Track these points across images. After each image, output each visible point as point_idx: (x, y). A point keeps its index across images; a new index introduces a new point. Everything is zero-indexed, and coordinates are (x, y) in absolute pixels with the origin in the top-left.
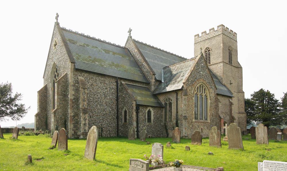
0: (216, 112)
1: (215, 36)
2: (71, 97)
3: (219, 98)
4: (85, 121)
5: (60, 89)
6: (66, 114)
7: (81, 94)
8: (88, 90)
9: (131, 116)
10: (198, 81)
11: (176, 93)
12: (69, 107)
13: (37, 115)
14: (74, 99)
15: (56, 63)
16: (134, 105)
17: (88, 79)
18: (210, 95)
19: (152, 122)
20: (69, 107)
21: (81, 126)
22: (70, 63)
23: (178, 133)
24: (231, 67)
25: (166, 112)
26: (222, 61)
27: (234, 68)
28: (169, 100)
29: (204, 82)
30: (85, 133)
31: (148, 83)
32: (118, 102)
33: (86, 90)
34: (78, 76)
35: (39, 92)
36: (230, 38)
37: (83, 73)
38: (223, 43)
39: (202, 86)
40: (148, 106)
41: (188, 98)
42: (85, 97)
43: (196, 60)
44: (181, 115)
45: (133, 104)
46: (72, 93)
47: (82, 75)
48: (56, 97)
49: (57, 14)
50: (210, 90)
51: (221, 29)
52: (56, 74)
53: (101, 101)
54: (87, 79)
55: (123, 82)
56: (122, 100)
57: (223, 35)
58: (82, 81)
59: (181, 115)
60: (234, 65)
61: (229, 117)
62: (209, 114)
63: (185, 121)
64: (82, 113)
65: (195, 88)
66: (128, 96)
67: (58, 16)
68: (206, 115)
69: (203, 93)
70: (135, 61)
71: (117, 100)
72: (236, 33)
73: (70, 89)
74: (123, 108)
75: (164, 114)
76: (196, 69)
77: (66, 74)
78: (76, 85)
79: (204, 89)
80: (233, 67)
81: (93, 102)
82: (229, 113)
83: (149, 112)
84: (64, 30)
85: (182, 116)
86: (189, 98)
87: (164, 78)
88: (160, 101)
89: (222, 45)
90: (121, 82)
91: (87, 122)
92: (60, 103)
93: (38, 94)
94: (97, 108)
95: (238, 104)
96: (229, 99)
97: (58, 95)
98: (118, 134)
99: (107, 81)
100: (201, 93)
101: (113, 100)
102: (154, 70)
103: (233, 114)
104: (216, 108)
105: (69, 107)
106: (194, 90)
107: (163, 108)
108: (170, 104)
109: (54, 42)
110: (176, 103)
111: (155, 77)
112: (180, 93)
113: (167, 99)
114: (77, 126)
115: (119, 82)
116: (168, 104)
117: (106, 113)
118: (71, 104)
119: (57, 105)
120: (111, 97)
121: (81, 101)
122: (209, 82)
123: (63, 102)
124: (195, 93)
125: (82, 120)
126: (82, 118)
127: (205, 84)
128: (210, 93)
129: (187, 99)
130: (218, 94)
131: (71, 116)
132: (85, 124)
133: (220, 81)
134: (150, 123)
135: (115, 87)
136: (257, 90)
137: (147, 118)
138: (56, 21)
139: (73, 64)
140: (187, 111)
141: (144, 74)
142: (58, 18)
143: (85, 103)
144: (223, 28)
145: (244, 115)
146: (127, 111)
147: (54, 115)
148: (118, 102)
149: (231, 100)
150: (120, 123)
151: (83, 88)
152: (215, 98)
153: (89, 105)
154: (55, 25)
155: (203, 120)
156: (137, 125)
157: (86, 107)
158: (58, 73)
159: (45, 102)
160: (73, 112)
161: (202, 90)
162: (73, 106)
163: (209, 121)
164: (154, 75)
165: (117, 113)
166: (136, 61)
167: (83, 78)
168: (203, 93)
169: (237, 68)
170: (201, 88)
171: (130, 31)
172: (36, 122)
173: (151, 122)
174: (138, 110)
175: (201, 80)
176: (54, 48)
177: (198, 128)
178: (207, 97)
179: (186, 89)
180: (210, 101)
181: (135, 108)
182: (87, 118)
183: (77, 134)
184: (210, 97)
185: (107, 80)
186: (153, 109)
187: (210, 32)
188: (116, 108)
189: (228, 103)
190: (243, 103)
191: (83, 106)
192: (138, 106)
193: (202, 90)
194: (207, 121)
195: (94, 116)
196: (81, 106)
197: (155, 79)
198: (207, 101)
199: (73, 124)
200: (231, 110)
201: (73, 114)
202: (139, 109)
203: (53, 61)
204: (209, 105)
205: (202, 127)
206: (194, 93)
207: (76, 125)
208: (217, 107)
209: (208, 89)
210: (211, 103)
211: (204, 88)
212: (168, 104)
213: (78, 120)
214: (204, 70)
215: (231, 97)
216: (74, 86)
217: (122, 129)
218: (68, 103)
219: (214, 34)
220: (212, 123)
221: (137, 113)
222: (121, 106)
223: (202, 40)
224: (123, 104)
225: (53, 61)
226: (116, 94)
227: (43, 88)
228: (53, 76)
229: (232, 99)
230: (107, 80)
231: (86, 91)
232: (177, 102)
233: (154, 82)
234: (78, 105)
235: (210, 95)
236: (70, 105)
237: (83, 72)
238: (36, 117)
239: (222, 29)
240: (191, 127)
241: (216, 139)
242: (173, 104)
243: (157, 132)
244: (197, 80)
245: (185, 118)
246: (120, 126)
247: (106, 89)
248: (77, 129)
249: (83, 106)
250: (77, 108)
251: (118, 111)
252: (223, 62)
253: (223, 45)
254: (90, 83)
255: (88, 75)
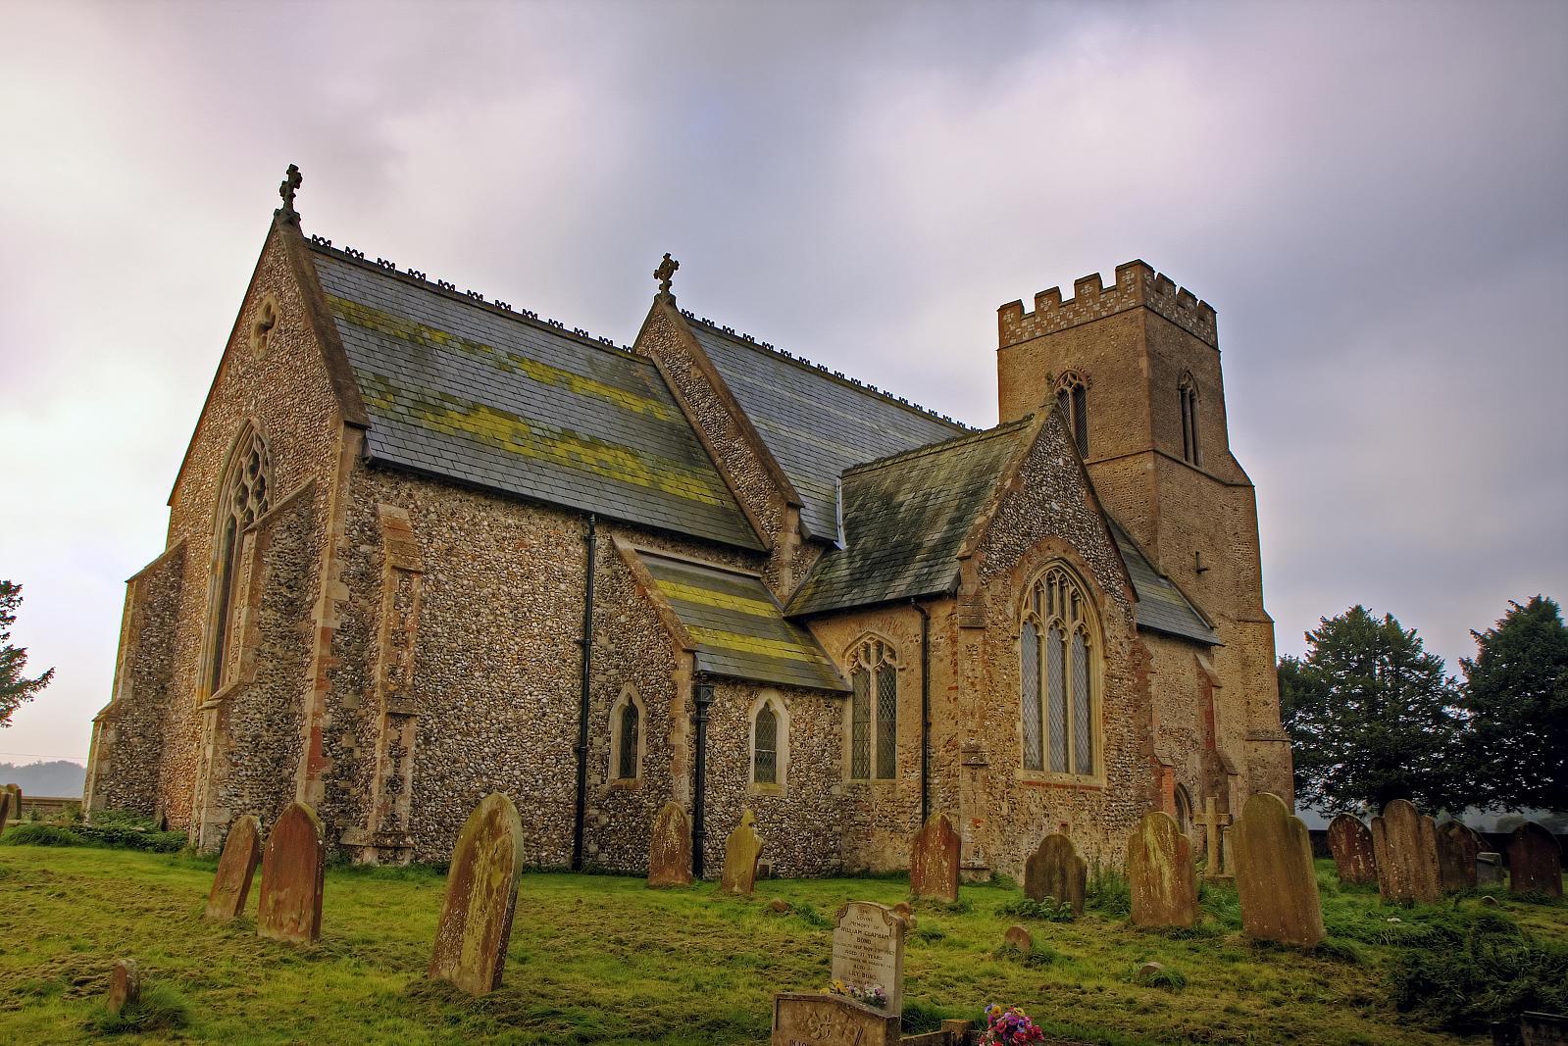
0: (1139, 727)
1: (1104, 314)
2: (326, 615)
3: (1152, 646)
4: (397, 766)
5: (268, 571)
6: (289, 717)
7: (385, 602)
8: (426, 581)
9: (665, 739)
10: (1040, 550)
11: (922, 612)
12: (308, 677)
13: (106, 719)
14: (342, 631)
15: (255, 421)
16: (683, 676)
17: (433, 516)
18: (1103, 629)
19: (782, 776)
20: (312, 673)
21: (367, 791)
22: (343, 426)
23: (943, 848)
24: (1194, 479)
25: (859, 724)
26: (1147, 446)
27: (1213, 484)
28: (880, 653)
29: (1070, 558)
30: (390, 836)
31: (760, 556)
32: (586, 657)
33: (416, 579)
34: (376, 501)
35: (136, 583)
36: (1185, 330)
37: (409, 485)
38: (1149, 354)
39: (1058, 576)
40: (763, 685)
41: (985, 643)
42: (411, 619)
43: (1022, 434)
44: (951, 744)
45: (676, 667)
46: (334, 596)
47: (397, 496)
48: (240, 615)
49: (293, 171)
50: (1103, 604)
51: (1134, 281)
52: (250, 483)
53: (492, 649)
54: (425, 516)
55: (624, 544)
56: (612, 647)
57: (1145, 314)
58: (395, 527)
59: (951, 744)
60: (1211, 473)
61: (1197, 757)
62: (1104, 739)
63: (974, 780)
64: (382, 715)
65: (1025, 587)
66: (651, 624)
67: (294, 178)
68: (1084, 743)
69: (1068, 616)
70: (692, 428)
71: (584, 645)
72: (1211, 309)
73: (324, 574)
74: (618, 691)
75: (849, 732)
76: (1026, 487)
77: (309, 486)
78: (363, 548)
79: (1073, 597)
80: (1204, 482)
81: (450, 652)
82: (1197, 736)
83: (767, 718)
84: (320, 248)
85: (956, 746)
86: (994, 646)
87: (847, 527)
88: (826, 656)
89: (1144, 363)
90: (611, 540)
91: (408, 771)
92: (259, 653)
93: (132, 597)
94: (467, 690)
95: (1246, 684)
96: (1197, 659)
97: (255, 606)
98: (579, 848)
99: (537, 528)
100: (1053, 617)
101: (563, 642)
102: (792, 482)
103: (1220, 739)
104: (1138, 707)
105: (308, 677)
106: (1021, 600)
107: (843, 695)
108: (888, 675)
109: (260, 311)
110: (919, 672)
111: (800, 521)
112: (941, 612)
113: (867, 647)
114: (345, 792)
115: (598, 542)
116: (873, 678)
117: (518, 721)
118: (322, 659)
119: (242, 664)
120: (549, 623)
121: (380, 642)
122: (1096, 560)
123: (277, 649)
124: (1025, 614)
125: (378, 755)
126: (379, 744)
127: (1075, 570)
128: (1104, 617)
129: (985, 652)
130: (1142, 629)
131: (315, 731)
132: (394, 784)
133: (1144, 554)
134: (772, 786)
135: (575, 568)
136: (1340, 611)
137: (752, 755)
138: (280, 204)
139: (357, 436)
140: (983, 717)
141: (737, 503)
142: (295, 190)
143: (406, 656)
144: (1144, 281)
145: (1278, 746)
146: (642, 714)
147: (219, 723)
148: (586, 657)
149: (1205, 663)
150: (594, 779)
151: (400, 570)
152: (1128, 648)
153: (423, 665)
154: (274, 223)
155: (1067, 771)
156: (697, 793)
157: (409, 681)
158: (262, 480)
159: (162, 642)
160: (328, 706)
161: (1062, 599)
162: (334, 672)
163: (1104, 783)
164: (796, 506)
165: (583, 722)
166: (695, 426)
167: (404, 514)
168: (1068, 616)
169: (1227, 490)
170: (1056, 590)
171: (667, 268)
172: (101, 759)
173: (773, 780)
174: (706, 705)
175: (1053, 545)
176: (253, 342)
177: (1045, 820)
178: (1086, 638)
179: (978, 595)
180: (1102, 665)
181: (686, 693)
182: (410, 743)
183: (342, 841)
184: (1104, 641)
185: (533, 528)
186: (788, 702)
187: (1037, 305)
188: (578, 693)
189: (1190, 680)
190: (1271, 682)
191: (393, 673)
192: (705, 681)
193: (1062, 599)
194: (1093, 781)
195: (450, 737)
196: (378, 673)
197: (801, 529)
198: (1087, 664)
199: (327, 777)
200: (1210, 716)
201: (328, 717)
202: (713, 698)
203: (238, 412)
204: (1102, 688)
205: (1066, 817)
206: (1019, 615)
207: (342, 784)
208: (1140, 701)
209: (1091, 594)
210: (1110, 676)
211: (1071, 589)
212: (873, 678)
213: (357, 754)
214: (1065, 489)
215: (1204, 646)
216: (350, 554)
217: (605, 820)
218: (308, 651)
219: (1103, 305)
220: (1118, 792)
221: (699, 724)
222: (603, 678)
223: (1038, 334)
224: (617, 667)
225: (238, 412)
226: (581, 607)
227: (163, 559)
228: (232, 493)
229: (1210, 657)
230: (533, 528)
231: (414, 585)
232: (925, 663)
233: (796, 548)
234: (362, 667)
235: (1103, 629)
236: (315, 665)
237: (405, 480)
238: (105, 727)
239: (1139, 284)
240: (1005, 811)
241: (1167, 884)
242: (903, 674)
243: (808, 839)
244: (1036, 545)
245: (973, 760)
246: (592, 797)
247: (528, 576)
248: (343, 811)
249: (393, 673)
250: (352, 682)
251: (584, 705)
252: (1155, 451)
253: (1153, 367)
254: (437, 543)
255: (431, 494)
